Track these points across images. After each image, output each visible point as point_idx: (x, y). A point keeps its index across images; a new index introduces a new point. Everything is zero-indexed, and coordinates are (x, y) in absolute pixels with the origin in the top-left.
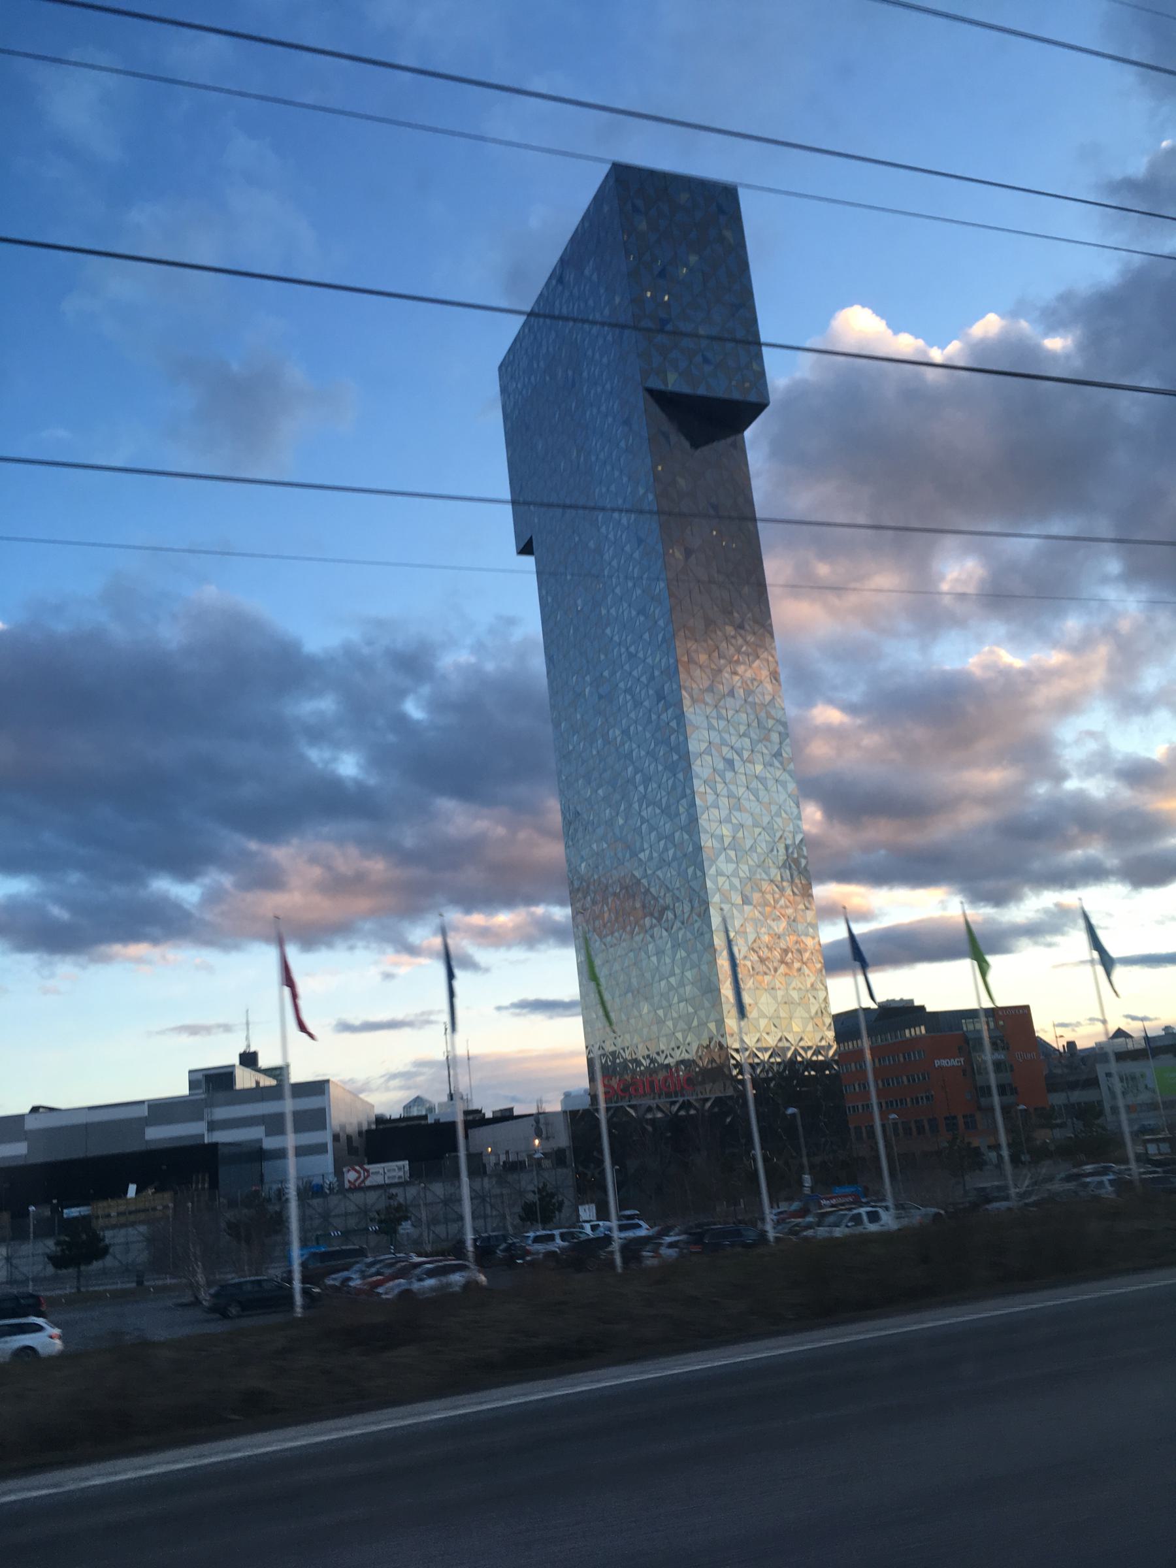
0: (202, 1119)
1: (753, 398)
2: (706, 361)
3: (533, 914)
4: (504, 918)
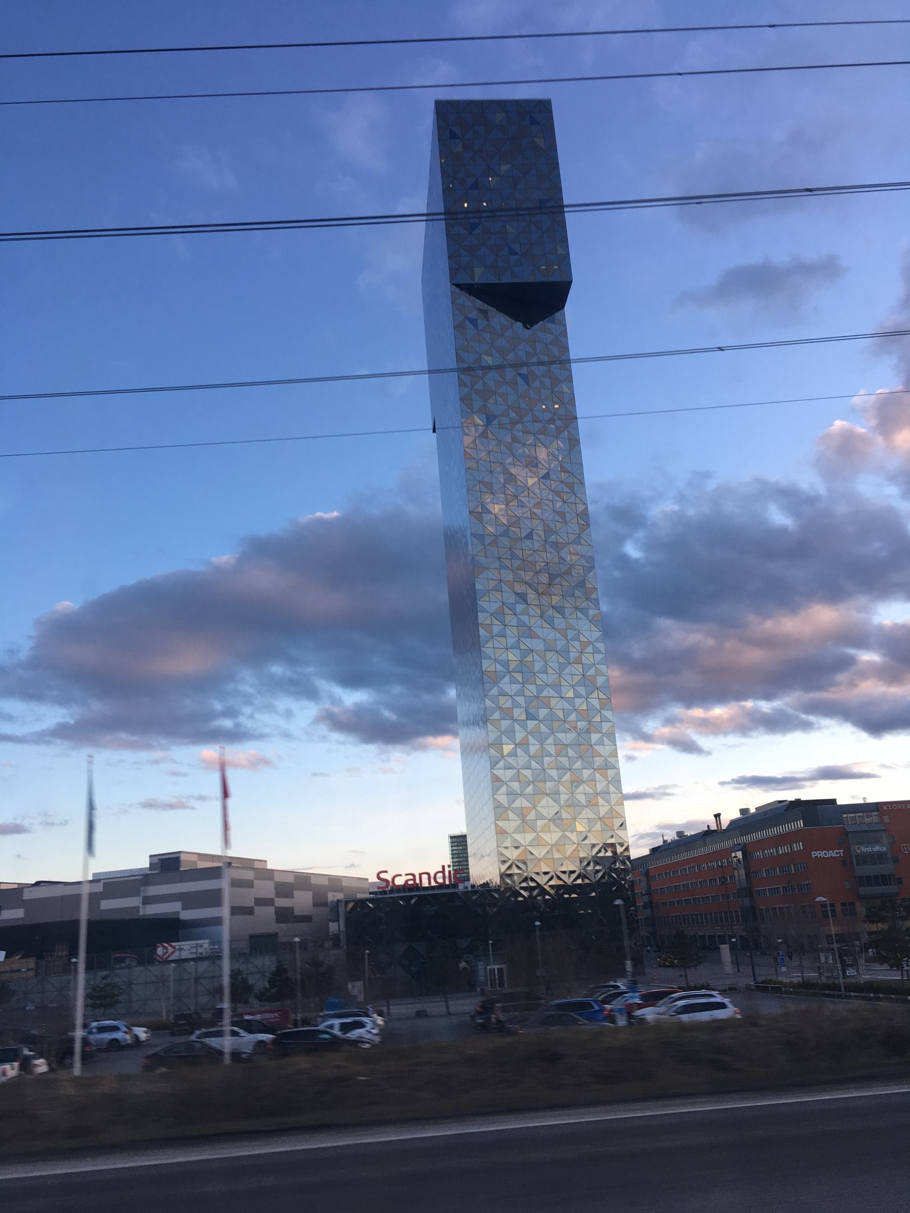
0: (138, 895)
1: (565, 279)
2: (512, 252)
3: (743, 708)
4: (719, 711)
